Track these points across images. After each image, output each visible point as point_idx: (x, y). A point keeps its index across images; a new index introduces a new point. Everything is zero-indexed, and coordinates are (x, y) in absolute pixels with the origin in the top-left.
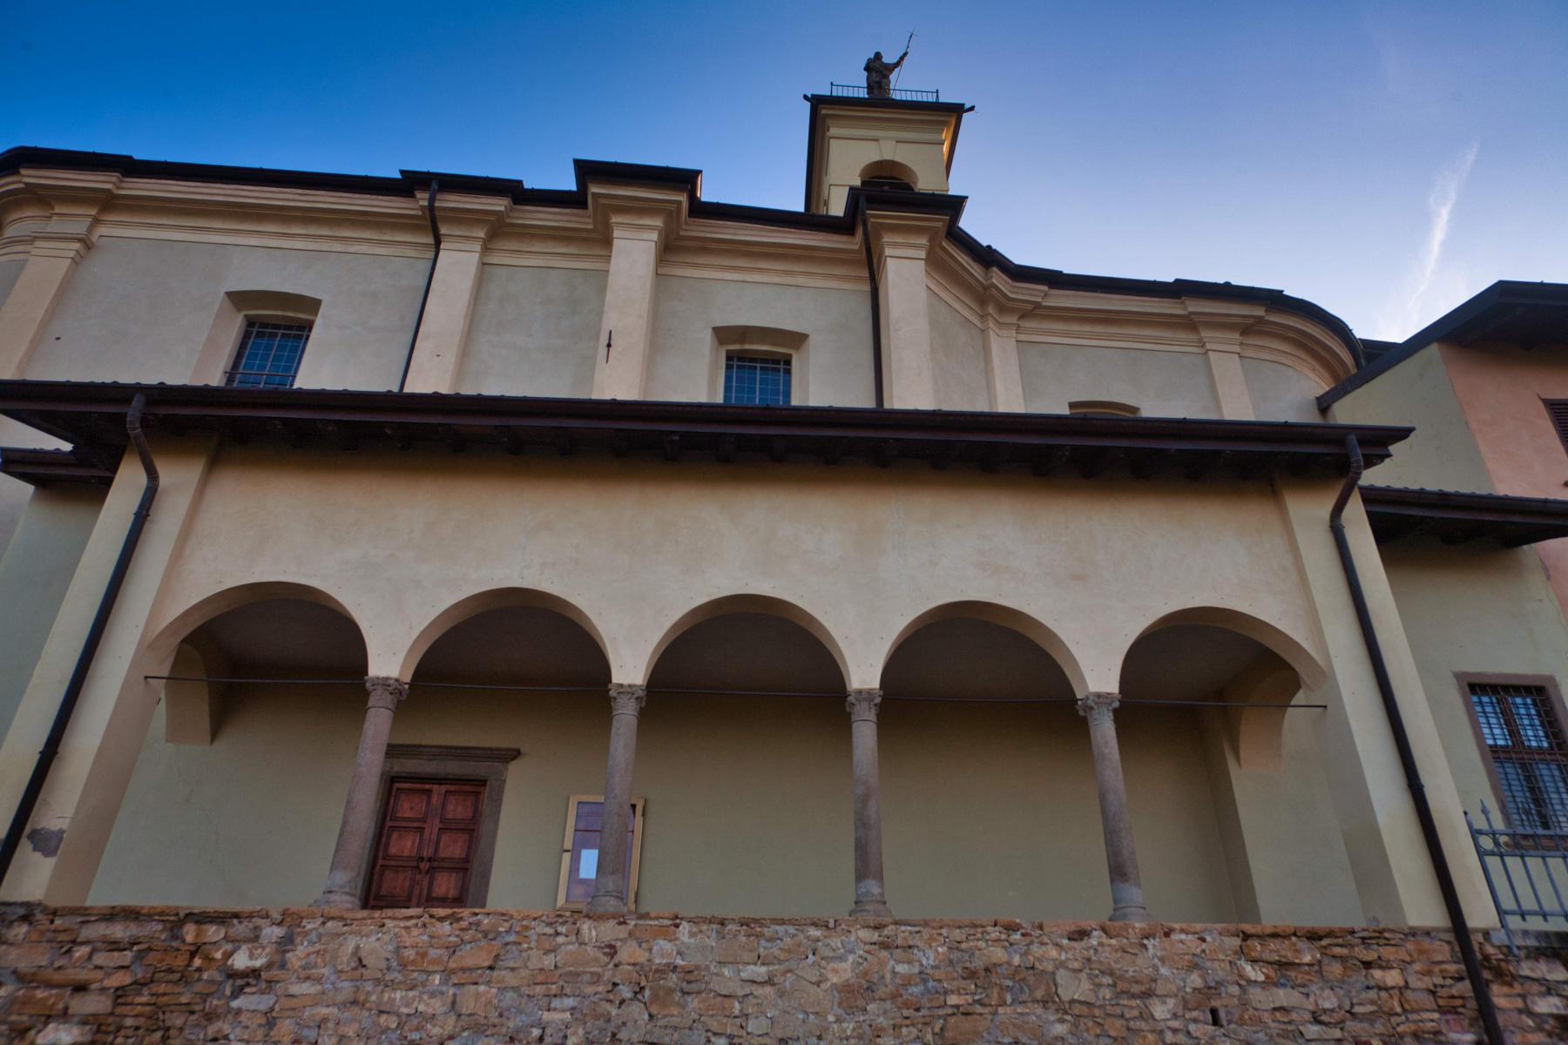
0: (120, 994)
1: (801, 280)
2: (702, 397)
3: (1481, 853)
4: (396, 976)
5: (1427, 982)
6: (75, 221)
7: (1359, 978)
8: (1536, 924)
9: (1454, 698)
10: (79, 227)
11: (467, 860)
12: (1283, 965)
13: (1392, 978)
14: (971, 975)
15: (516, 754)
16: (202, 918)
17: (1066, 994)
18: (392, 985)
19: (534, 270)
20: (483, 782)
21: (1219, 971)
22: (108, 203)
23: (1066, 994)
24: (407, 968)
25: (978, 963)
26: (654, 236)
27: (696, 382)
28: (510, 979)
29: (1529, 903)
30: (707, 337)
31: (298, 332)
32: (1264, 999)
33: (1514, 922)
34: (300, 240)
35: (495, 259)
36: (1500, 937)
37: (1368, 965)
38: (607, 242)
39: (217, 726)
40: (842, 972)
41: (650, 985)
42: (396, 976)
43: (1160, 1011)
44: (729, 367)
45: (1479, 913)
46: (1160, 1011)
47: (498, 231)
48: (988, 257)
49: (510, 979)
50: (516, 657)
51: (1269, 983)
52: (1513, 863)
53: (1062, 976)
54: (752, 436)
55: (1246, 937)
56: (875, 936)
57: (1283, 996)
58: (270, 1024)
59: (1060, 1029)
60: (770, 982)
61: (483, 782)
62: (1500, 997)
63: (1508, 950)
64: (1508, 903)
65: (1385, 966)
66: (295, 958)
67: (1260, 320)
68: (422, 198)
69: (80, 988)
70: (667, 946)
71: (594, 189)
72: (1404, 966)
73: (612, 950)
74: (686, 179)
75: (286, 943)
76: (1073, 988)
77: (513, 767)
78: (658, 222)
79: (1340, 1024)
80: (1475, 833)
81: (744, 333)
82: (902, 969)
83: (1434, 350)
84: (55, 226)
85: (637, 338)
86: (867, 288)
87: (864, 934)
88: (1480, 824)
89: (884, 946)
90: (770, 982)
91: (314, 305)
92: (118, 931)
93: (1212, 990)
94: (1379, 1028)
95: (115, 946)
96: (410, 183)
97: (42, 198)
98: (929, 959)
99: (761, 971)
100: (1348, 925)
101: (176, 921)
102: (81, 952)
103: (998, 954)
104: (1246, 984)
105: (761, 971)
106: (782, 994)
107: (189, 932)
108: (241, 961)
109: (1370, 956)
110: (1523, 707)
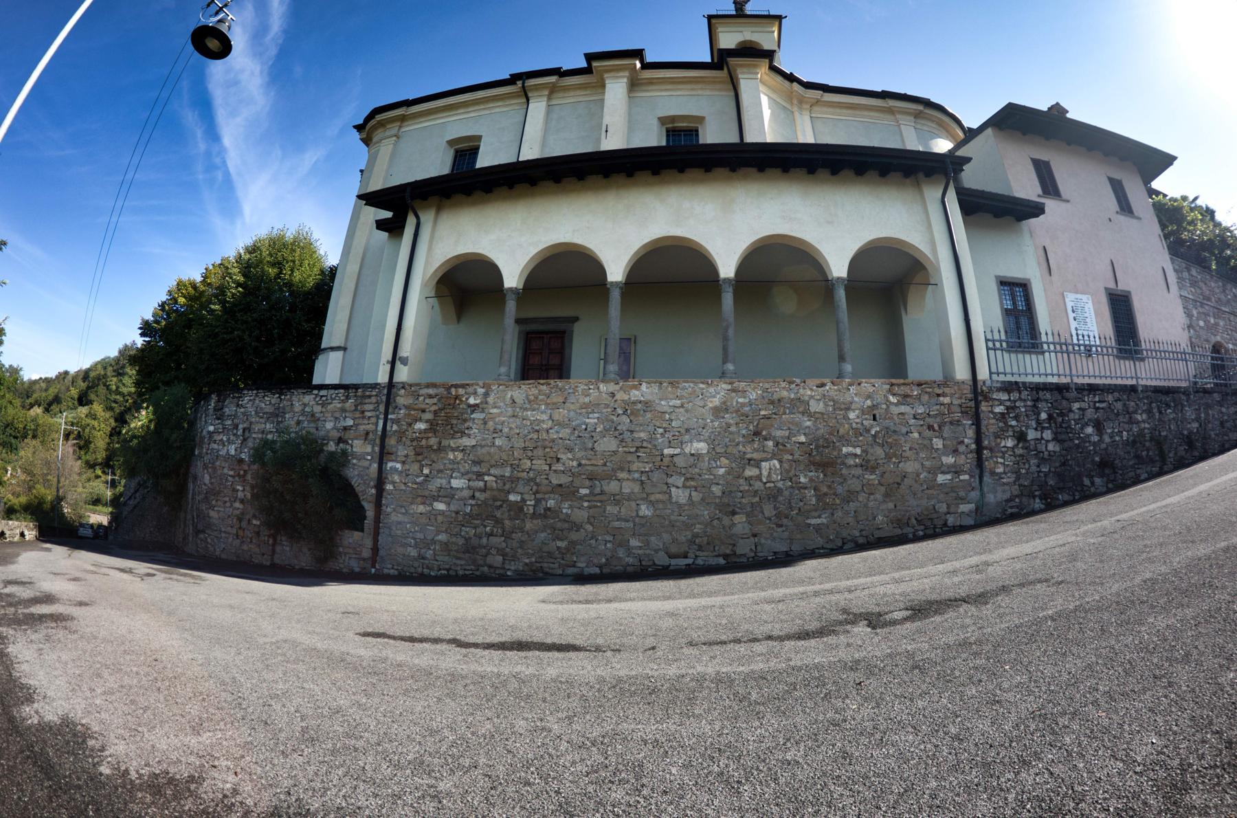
0: (435, 412)
1: (700, 92)
2: (654, 144)
3: (988, 349)
4: (528, 406)
5: (959, 402)
6: (393, 129)
7: (933, 400)
8: (1002, 378)
9: (993, 287)
10: (394, 131)
11: (561, 365)
12: (906, 396)
13: (947, 400)
14: (772, 402)
15: (576, 319)
16: (456, 386)
17: (812, 410)
18: (526, 409)
19: (572, 101)
20: (564, 332)
21: (879, 399)
22: (403, 119)
23: (812, 410)
24: (532, 403)
25: (776, 397)
26: (625, 80)
27: (652, 137)
28: (572, 407)
29: (1008, 370)
30: (655, 122)
31: (474, 151)
32: (895, 410)
33: (995, 377)
34: (473, 113)
35: (554, 102)
36: (988, 383)
37: (938, 395)
38: (603, 86)
39: (459, 319)
40: (716, 401)
41: (630, 409)
42: (528, 406)
43: (852, 415)
44: (668, 136)
45: (983, 374)
46: (852, 415)
47: (553, 90)
48: (791, 78)
49: (572, 407)
50: (567, 273)
51: (898, 404)
52: (1006, 355)
53: (812, 403)
54: (682, 157)
55: (892, 385)
56: (729, 387)
57: (903, 409)
58: (485, 423)
59: (808, 423)
60: (682, 406)
61: (564, 332)
62: (984, 407)
63: (990, 388)
64: (994, 370)
65: (944, 395)
66: (490, 400)
67: (921, 112)
68: (519, 83)
69: (423, 411)
70: (637, 393)
71: (595, 64)
72: (952, 396)
73: (613, 395)
74: (638, 54)
75: (486, 395)
76: (816, 407)
77: (576, 324)
78: (627, 74)
79: (923, 419)
80: (987, 340)
81: (673, 119)
82: (741, 400)
83: (989, 131)
84: (388, 133)
85: (622, 119)
86: (732, 93)
87: (724, 386)
88: (989, 337)
89: (733, 390)
90: (682, 406)
91: (479, 138)
92: (431, 391)
93: (874, 407)
94: (938, 420)
95: (431, 397)
96: (514, 79)
97: (382, 124)
98: (753, 396)
99: (678, 402)
100: (933, 378)
101: (448, 388)
102: (421, 399)
103: (785, 394)
104: (889, 403)
105: (678, 402)
106: (687, 411)
107: (453, 391)
108: (472, 401)
109: (939, 391)
110: (1019, 291)
